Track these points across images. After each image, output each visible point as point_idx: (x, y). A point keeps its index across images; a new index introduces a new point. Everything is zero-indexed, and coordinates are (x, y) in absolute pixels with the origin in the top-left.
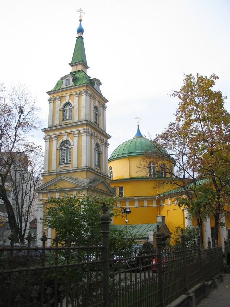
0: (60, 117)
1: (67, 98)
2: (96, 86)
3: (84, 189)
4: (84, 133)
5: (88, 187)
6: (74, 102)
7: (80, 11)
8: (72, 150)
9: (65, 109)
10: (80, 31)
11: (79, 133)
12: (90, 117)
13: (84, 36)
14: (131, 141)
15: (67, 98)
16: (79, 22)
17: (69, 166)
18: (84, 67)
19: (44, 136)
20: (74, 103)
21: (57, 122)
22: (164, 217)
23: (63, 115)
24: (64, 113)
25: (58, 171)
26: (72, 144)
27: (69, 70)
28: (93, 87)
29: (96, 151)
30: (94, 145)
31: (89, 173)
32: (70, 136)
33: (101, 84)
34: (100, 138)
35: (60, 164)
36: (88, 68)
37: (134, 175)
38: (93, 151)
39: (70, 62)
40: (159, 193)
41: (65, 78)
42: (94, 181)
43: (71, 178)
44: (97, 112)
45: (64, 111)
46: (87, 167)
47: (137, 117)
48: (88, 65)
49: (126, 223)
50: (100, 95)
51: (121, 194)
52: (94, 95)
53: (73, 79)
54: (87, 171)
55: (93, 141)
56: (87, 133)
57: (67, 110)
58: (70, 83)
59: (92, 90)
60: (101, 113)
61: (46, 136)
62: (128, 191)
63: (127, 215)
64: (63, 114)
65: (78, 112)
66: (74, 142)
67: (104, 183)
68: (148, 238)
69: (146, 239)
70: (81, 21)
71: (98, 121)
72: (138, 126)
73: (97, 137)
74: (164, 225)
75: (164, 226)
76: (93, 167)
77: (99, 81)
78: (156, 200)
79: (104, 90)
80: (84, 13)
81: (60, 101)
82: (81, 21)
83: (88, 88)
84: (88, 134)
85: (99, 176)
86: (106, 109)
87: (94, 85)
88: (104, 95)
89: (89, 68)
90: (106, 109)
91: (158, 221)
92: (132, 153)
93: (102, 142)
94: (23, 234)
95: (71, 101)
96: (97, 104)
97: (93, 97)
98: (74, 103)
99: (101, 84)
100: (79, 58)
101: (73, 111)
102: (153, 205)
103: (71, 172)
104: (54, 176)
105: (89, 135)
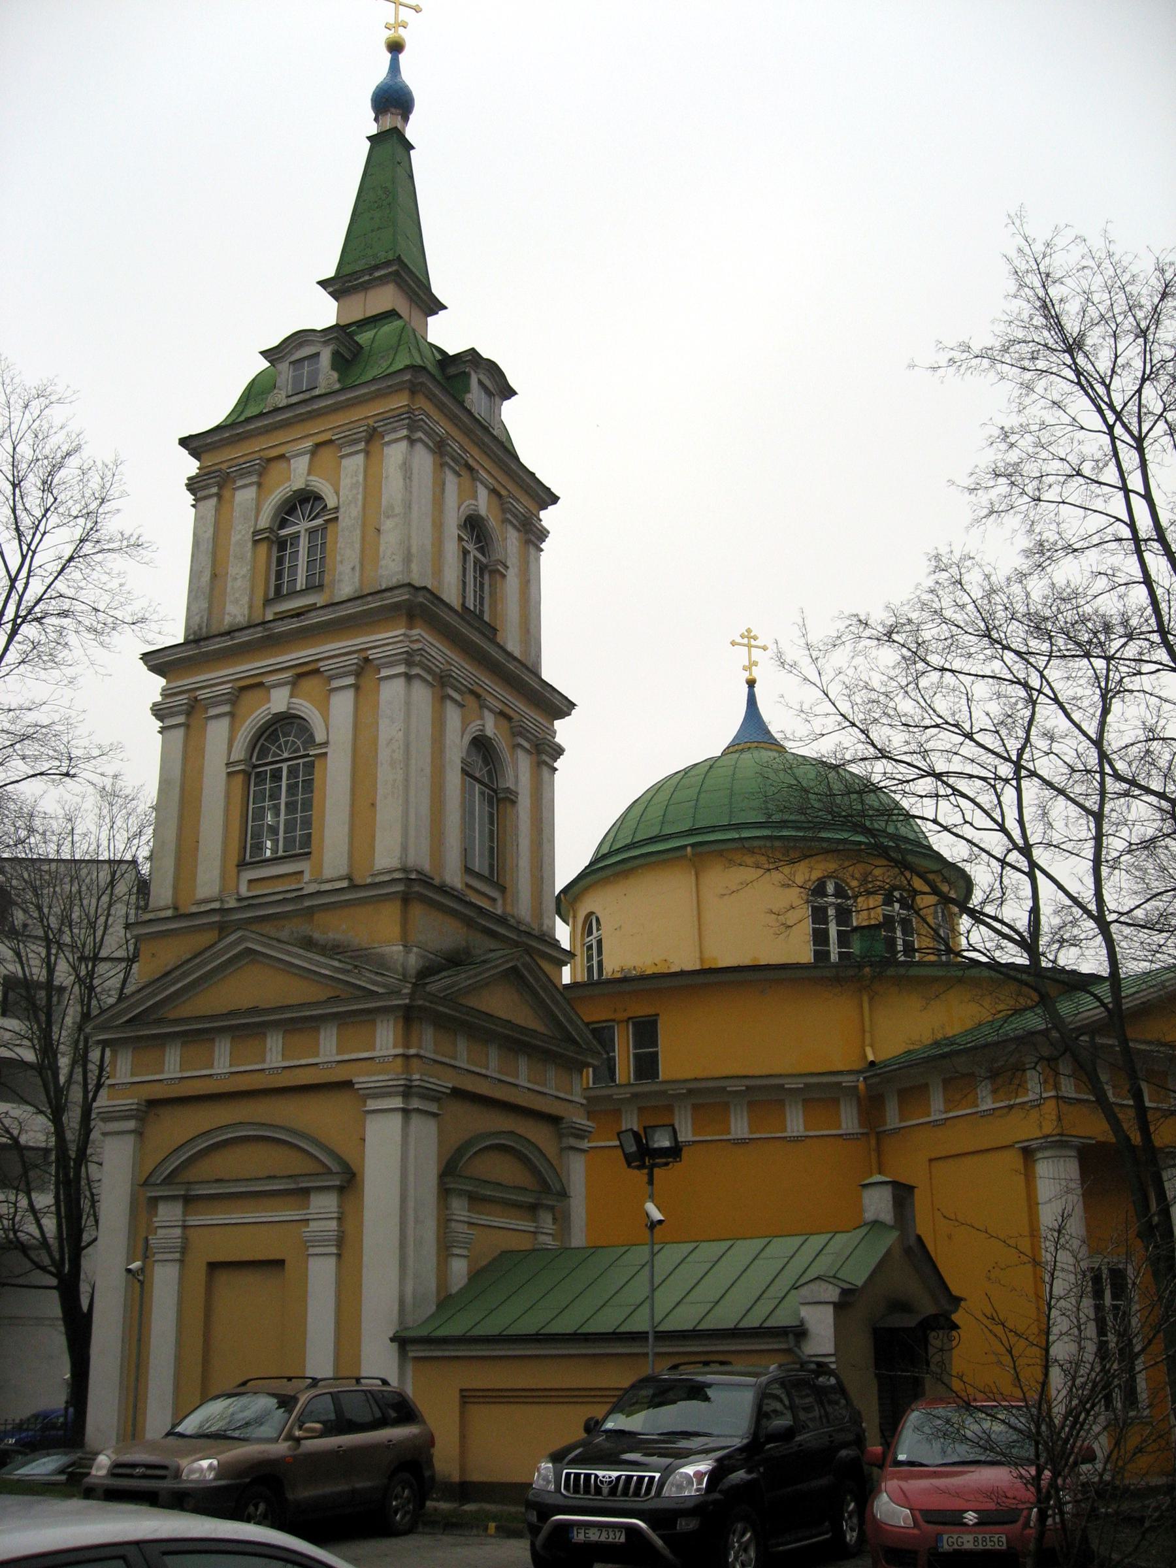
0: (253, 579)
1: (300, 465)
2: (475, 398)
3: (385, 1010)
4: (391, 665)
5: (412, 996)
6: (343, 483)
8: (317, 775)
9: (283, 532)
10: (393, 101)
12: (438, 571)
13: (411, 133)
14: (711, 767)
15: (300, 465)
17: (302, 872)
18: (411, 300)
19: (159, 699)
20: (337, 493)
21: (236, 611)
22: (911, 1189)
24: (280, 561)
25: (232, 903)
26: (319, 737)
28: (461, 404)
29: (477, 786)
31: (417, 910)
32: (308, 684)
33: (509, 392)
34: (500, 706)
36: (435, 306)
37: (727, 957)
38: (454, 779)
39: (331, 273)
40: (874, 1053)
41: (291, 353)
42: (454, 960)
43: (309, 943)
44: (482, 550)
45: (282, 545)
46: (404, 870)
47: (742, 636)
48: (438, 289)
49: (653, 1225)
50: (502, 451)
51: (647, 1066)
52: (458, 442)
53: (336, 355)
54: (406, 899)
55: (453, 716)
56: (409, 663)
57: (296, 536)
58: (321, 377)
59: (453, 419)
60: (513, 561)
61: (165, 693)
62: (693, 1048)
63: (656, 1170)
64: (274, 560)
65: (358, 546)
66: (334, 719)
67: (521, 977)
68: (800, 1333)
69: (791, 1336)
70: (395, 47)
71: (494, 605)
72: (751, 683)
73: (478, 696)
74: (912, 1241)
75: (908, 1251)
76: (454, 877)
77: (493, 369)
78: (859, 1098)
79: (532, 429)
81: (254, 489)
82: (395, 47)
83: (422, 402)
84: (416, 671)
85: (493, 934)
86: (543, 546)
87: (468, 391)
88: (529, 456)
89: (445, 308)
90: (543, 546)
91: (869, 1216)
92: (713, 829)
93: (518, 731)
94: (85, 1308)
96: (483, 503)
97: (453, 459)
98: (337, 493)
99: (509, 392)
100: (383, 250)
101: (329, 539)
102: (839, 1127)
103: (307, 907)
105: (425, 680)
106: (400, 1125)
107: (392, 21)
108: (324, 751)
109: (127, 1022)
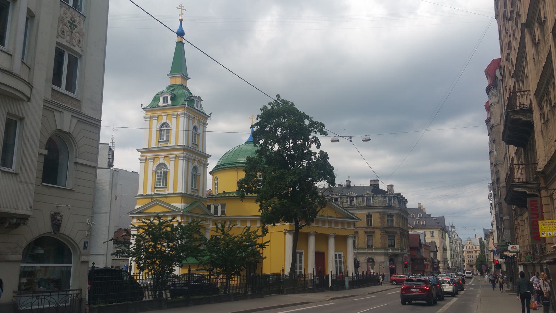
1: (165, 117)
11: (176, 157)
15: (165, 117)
21: (154, 145)
27: (168, 82)
30: (191, 128)
35: (155, 188)
48: (189, 76)
66: (171, 166)
70: (181, 20)
80: (185, 10)
104: (149, 200)
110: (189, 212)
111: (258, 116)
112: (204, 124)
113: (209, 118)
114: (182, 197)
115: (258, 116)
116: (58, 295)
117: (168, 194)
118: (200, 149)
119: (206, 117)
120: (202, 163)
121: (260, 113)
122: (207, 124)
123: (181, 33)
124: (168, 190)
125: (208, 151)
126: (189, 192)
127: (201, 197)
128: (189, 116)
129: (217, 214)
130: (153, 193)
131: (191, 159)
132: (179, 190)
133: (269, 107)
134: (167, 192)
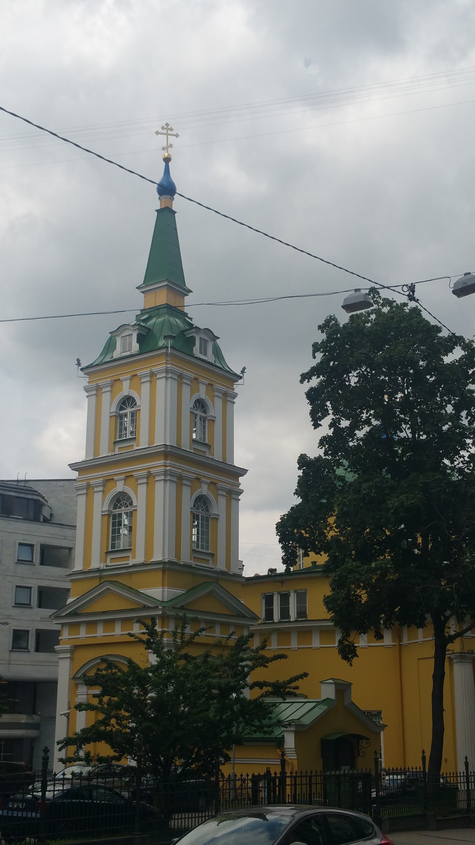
1: (126, 384)
7: (165, 131)
11: (149, 476)
15: (126, 384)
16: (164, 164)
21: (104, 452)
23: (118, 427)
28: (193, 356)
30: (188, 404)
32: (130, 480)
45: (121, 417)
53: (139, 336)
57: (126, 415)
66: (139, 498)
70: (167, 160)
80: (177, 136)
95: (134, 394)
106: (161, 576)
107: (165, 146)
108: (139, 408)
109: (66, 615)
110: (182, 608)
111: (316, 348)
112: (225, 395)
113: (240, 381)
114: (164, 570)
115: (316, 348)
116: (321, 784)
117: (134, 566)
118: (217, 455)
119: (235, 378)
120: (222, 489)
121: (321, 337)
122: (235, 396)
123: (167, 189)
124: (134, 557)
125: (239, 460)
126: (186, 558)
127: (222, 573)
128: (181, 376)
129: (289, 617)
130: (102, 566)
131: (188, 479)
132: (157, 557)
133: (344, 318)
134: (131, 562)
